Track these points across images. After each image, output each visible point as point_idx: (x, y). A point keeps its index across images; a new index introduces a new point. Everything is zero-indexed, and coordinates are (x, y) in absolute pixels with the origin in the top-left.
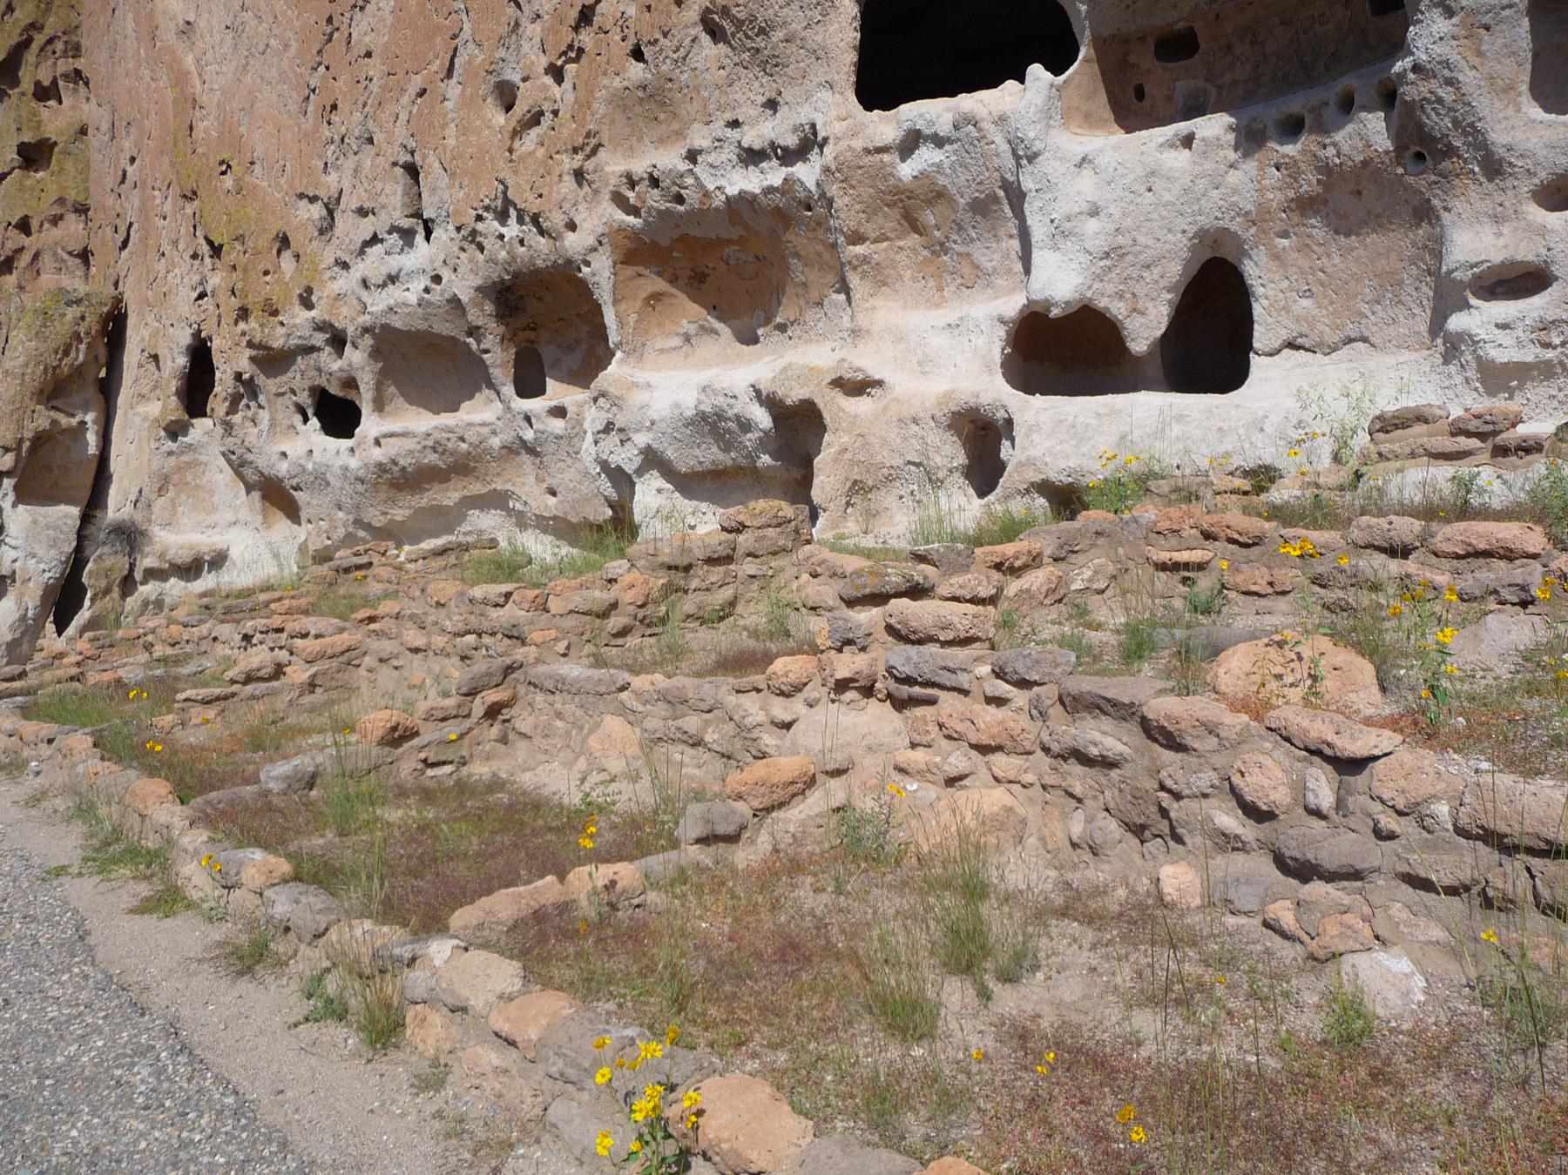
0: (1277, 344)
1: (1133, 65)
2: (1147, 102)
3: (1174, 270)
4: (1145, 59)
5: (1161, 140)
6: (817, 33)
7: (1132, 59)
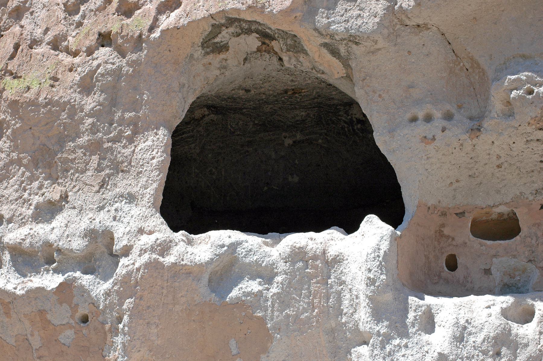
1: (448, 237)
2: (459, 272)
5: (504, 306)
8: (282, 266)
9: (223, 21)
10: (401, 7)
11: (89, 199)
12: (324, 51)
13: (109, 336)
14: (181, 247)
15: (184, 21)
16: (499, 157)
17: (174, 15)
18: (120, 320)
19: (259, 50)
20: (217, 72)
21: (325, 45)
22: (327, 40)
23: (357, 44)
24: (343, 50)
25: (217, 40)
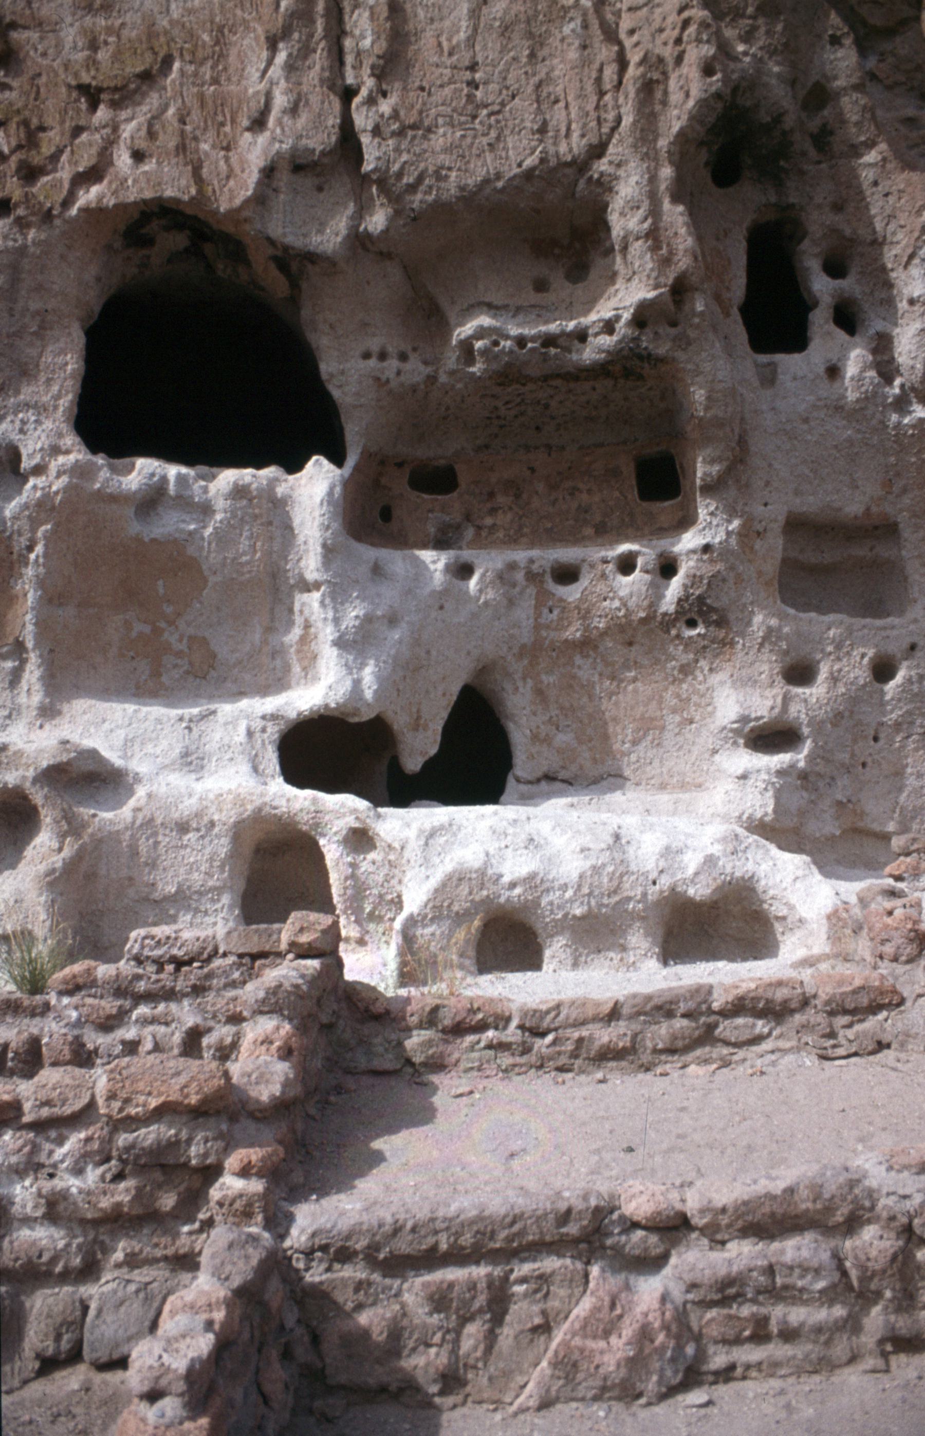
0: (539, 774)
3: (455, 689)
4: (399, 484)
6: (32, 344)
7: (384, 481)
8: (220, 504)
9: (156, 210)
10: (366, 229)
11: (230, 1403)
12: (272, 266)
13: (17, 565)
14: (105, 474)
15: (110, 202)
16: (448, 409)
17: (95, 190)
18: (30, 549)
19: (186, 250)
20: (135, 270)
21: (275, 259)
22: (279, 253)
23: (313, 263)
24: (294, 266)
25: (143, 231)
